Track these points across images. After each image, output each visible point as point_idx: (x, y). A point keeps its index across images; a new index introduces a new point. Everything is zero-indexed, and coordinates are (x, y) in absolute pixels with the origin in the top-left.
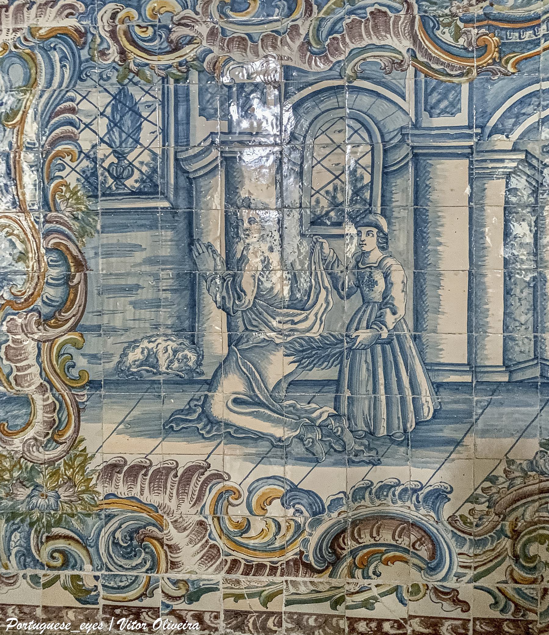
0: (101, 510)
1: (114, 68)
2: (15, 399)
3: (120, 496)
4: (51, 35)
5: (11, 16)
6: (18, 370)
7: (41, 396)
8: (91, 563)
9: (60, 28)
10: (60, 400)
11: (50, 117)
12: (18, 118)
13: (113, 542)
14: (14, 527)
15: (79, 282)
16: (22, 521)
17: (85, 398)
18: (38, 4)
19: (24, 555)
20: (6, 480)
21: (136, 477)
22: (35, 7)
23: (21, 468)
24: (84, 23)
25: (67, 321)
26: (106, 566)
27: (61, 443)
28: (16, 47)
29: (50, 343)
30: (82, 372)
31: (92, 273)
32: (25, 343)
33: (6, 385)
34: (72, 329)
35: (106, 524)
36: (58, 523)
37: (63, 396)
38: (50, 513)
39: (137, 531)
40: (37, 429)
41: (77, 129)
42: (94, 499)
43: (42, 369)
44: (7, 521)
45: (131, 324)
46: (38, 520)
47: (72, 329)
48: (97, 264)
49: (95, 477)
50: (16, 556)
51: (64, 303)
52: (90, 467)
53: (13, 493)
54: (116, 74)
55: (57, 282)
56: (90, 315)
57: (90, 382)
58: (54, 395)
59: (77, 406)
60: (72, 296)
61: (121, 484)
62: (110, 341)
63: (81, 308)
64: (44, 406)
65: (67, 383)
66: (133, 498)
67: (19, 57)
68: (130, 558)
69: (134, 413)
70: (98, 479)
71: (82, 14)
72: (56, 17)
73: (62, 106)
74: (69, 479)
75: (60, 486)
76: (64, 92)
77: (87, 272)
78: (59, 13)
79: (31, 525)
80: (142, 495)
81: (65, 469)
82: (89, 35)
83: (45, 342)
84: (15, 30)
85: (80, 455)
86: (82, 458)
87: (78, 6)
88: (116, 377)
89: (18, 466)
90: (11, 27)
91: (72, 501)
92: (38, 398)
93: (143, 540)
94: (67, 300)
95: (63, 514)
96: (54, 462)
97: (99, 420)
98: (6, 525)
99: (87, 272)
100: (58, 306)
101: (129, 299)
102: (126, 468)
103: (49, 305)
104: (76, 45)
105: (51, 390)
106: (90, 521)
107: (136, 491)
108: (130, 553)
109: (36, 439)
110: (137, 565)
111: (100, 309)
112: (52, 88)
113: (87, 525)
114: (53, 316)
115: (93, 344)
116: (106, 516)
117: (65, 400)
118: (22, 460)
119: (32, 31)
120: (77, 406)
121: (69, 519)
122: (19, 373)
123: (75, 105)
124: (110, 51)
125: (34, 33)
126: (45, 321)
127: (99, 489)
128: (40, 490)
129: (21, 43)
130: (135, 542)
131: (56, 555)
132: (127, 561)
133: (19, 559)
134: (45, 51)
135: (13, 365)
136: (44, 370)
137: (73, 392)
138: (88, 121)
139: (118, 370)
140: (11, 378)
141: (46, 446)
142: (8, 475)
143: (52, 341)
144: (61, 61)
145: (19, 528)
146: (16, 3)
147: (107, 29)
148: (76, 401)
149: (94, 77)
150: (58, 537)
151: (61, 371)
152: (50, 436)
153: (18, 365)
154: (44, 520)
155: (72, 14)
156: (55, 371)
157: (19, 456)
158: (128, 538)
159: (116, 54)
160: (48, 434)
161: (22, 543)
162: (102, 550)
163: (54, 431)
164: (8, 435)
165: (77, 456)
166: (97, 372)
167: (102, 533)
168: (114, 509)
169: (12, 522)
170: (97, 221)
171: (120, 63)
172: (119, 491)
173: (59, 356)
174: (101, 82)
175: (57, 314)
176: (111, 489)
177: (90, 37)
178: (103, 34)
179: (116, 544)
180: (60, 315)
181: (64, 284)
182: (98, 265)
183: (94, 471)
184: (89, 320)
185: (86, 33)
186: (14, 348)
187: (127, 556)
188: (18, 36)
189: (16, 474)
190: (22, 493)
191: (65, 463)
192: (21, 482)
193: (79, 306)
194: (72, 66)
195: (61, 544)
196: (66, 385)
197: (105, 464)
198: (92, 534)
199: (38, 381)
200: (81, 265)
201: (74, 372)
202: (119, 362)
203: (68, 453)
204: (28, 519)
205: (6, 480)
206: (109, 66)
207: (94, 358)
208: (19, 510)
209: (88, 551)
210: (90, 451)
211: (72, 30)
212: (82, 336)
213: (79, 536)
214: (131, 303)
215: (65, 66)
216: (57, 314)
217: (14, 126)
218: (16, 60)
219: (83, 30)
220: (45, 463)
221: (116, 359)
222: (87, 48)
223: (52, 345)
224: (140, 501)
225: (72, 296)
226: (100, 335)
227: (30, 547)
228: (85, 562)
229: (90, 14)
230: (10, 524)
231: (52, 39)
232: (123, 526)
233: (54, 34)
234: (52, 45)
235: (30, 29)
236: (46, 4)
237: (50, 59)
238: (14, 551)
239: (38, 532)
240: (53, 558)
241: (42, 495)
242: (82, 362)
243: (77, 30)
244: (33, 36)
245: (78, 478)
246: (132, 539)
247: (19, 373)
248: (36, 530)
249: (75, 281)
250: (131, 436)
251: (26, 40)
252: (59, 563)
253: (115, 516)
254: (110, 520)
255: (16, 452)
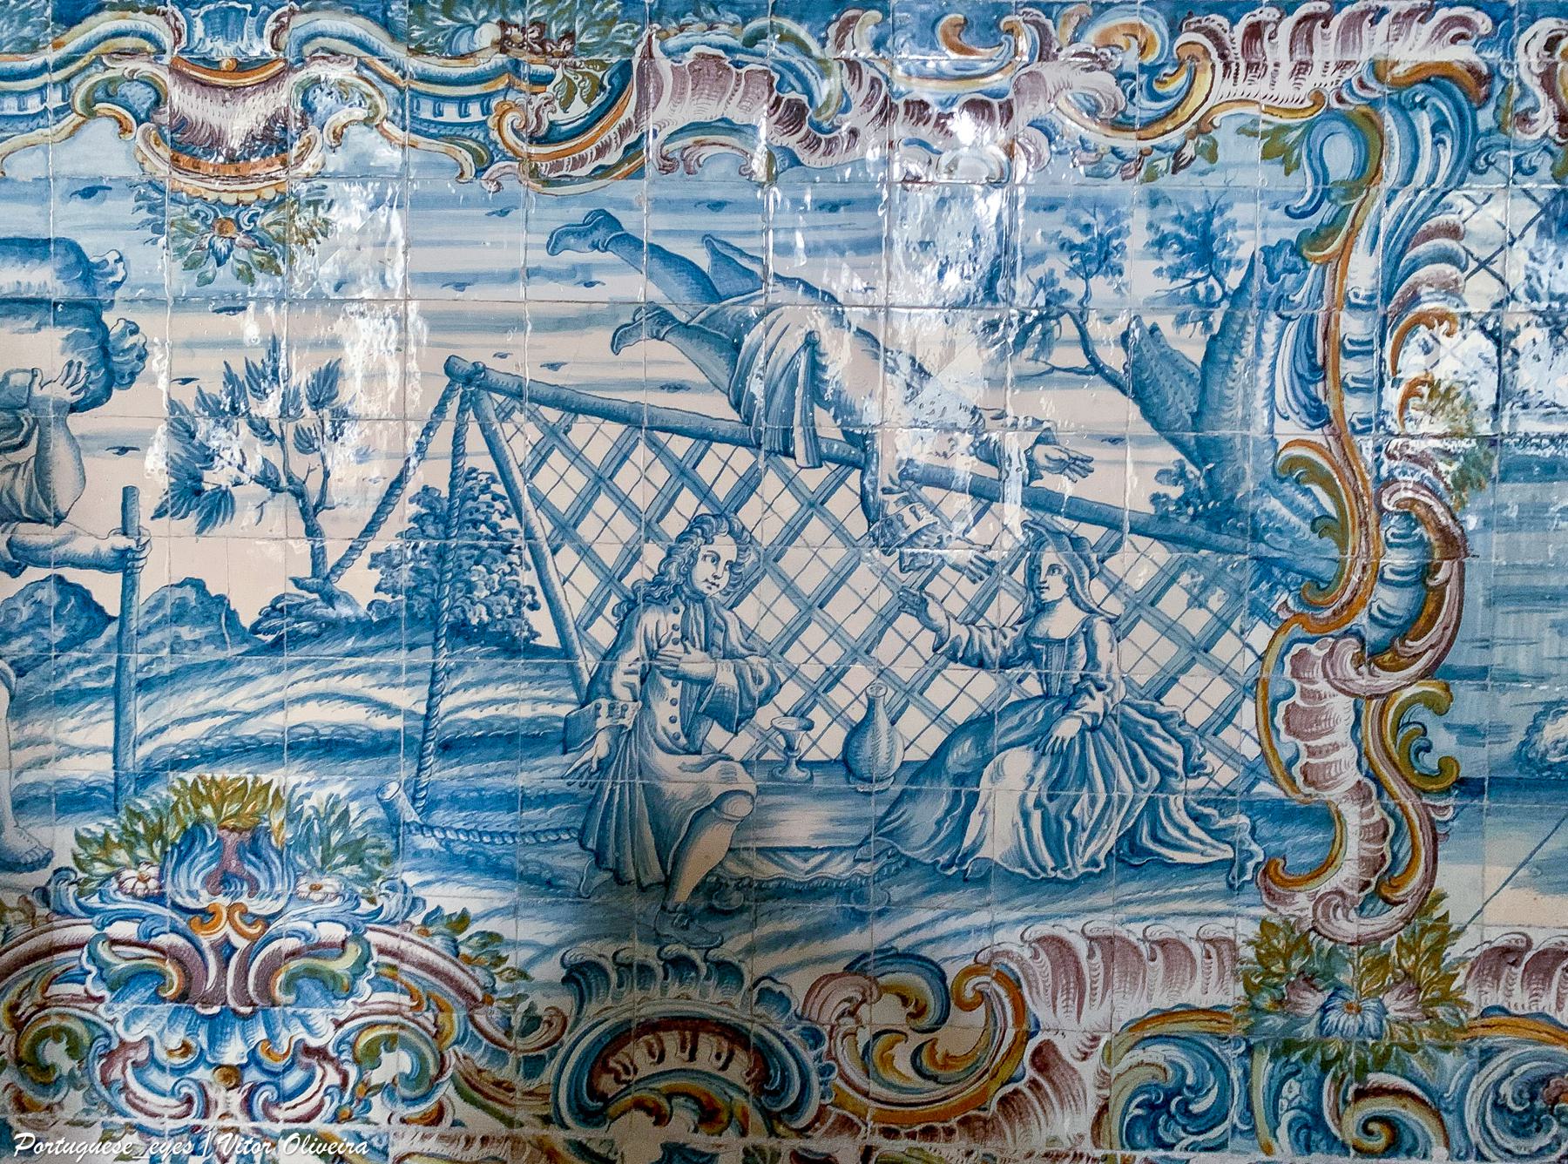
0: (1473, 1039)
1: (1546, 148)
2: (1301, 812)
3: (1513, 1010)
4: (1418, 76)
5: (1334, 36)
6: (1312, 754)
7: (1358, 808)
8: (1447, 1145)
9: (1438, 65)
10: (1398, 816)
11: (1406, 244)
12: (1337, 244)
13: (1495, 1104)
14: (1289, 1069)
15: (1447, 581)
16: (1306, 1058)
17: (1450, 814)
18: (1392, 14)
19: (1306, 1126)
20: (1275, 975)
21: (1549, 975)
22: (1386, 19)
23: (1308, 951)
24: (1489, 55)
25: (1420, 655)
26: (1479, 1151)
27: (1396, 904)
28: (1340, 100)
29: (1380, 701)
30: (1446, 763)
31: (1475, 561)
32: (1329, 700)
33: (1283, 783)
34: (1427, 674)
35: (1482, 1065)
36: (1381, 1064)
37: (1403, 808)
38: (1365, 1043)
39: (1545, 1081)
40: (1346, 874)
41: (1463, 270)
42: (1457, 1016)
43: (1362, 753)
44: (1274, 1057)
45: (1552, 667)
46: (1339, 1056)
47: (1427, 674)
48: (1487, 546)
49: (1463, 972)
50: (1290, 1127)
51: (1413, 619)
52: (1454, 951)
53: (1289, 1001)
54: (1549, 161)
55: (1398, 578)
56: (1467, 647)
57: (1461, 782)
58: (1385, 807)
59: (1433, 829)
60: (1431, 607)
61: (1517, 987)
62: (1506, 700)
63: (1449, 632)
64: (1363, 827)
65: (1414, 781)
66: (1541, 1015)
67: (1346, 119)
68: (1527, 1135)
69: (1548, 847)
70: (1468, 976)
71: (1487, 36)
72: (1430, 41)
73: (1432, 223)
74: (1407, 975)
75: (1388, 989)
76: (1438, 195)
77: (1466, 560)
78: (1438, 34)
79: (1325, 1066)
80: (1559, 1009)
81: (1400, 956)
82: (1497, 79)
83: (1370, 698)
84: (1342, 66)
85: (1433, 928)
86: (1435, 935)
87: (1479, 21)
88: (1515, 773)
89: (1303, 947)
90: (1333, 58)
91: (1411, 1020)
92: (1352, 815)
93: (1556, 1100)
94: (1420, 613)
95: (1391, 1045)
96: (1379, 940)
97: (1477, 857)
98: (1271, 1066)
99: (1466, 560)
100: (1400, 627)
101: (1552, 616)
102: (1528, 957)
103: (1384, 625)
104: (1469, 102)
105: (1380, 795)
106: (1448, 1060)
107: (1547, 1003)
108: (1529, 1123)
109: (1341, 893)
110: (1541, 1149)
111: (1487, 634)
112: (1412, 186)
113: (1443, 1071)
114: (1389, 647)
115: (1470, 703)
116: (1482, 1051)
117: (1408, 818)
118: (1313, 934)
119: (1378, 69)
120: (1433, 829)
121: (1404, 1054)
122: (1312, 761)
123: (1459, 223)
124: (1540, 115)
125: (1382, 73)
126: (1373, 656)
127: (1469, 996)
128: (1347, 995)
129: (1353, 93)
130: (1539, 1104)
131: (1373, 1126)
132: (1521, 1142)
133: (1297, 1135)
134: (1403, 109)
135: (1301, 744)
136: (1367, 754)
137: (1425, 800)
138: (1484, 254)
139: (1522, 756)
140: (1296, 770)
141: (1362, 908)
142: (1281, 965)
143: (1386, 697)
144: (1434, 131)
145: (1298, 1071)
146: (1347, 10)
147: (1538, 71)
148: (1431, 819)
149: (1502, 165)
150: (1380, 1091)
151: (1398, 756)
152: (1372, 888)
153: (1311, 743)
154: (1352, 1056)
155: (1462, 36)
156: (1390, 758)
157: (1306, 926)
158: (1526, 1095)
159: (1551, 120)
160: (1368, 884)
161: (1305, 1103)
162: (1470, 1118)
163: (1380, 885)
164: (1285, 883)
165: (1429, 928)
166: (1475, 761)
167: (1473, 1086)
168: (1497, 1038)
169: (1284, 1059)
170: (1492, 457)
171: (1559, 140)
172: (1513, 1001)
173: (1397, 727)
174: (1518, 176)
175: (1397, 643)
176: (1495, 997)
177: (1499, 86)
178: (1526, 78)
179: (1499, 1107)
180: (1403, 644)
181: (1415, 583)
182: (1491, 551)
183: (1462, 961)
184: (1463, 656)
185: (1491, 76)
186: (1304, 710)
187: (1520, 1131)
188: (1346, 77)
189: (1296, 964)
190: (1312, 1001)
191: (1401, 943)
192: (1305, 980)
193: (1446, 628)
194: (1457, 144)
195: (1384, 1106)
196: (1410, 785)
197: (1486, 946)
198: (1452, 1088)
199: (1352, 776)
200: (1454, 544)
201: (1430, 761)
202: (1523, 744)
203: (1408, 923)
204: (1318, 1055)
205: (1275, 975)
206: (1537, 143)
207: (1470, 733)
208: (1300, 1034)
209: (1441, 1121)
210: (1455, 921)
211: (1463, 69)
212: (1447, 689)
213: (1424, 1089)
214: (1553, 625)
215: (1442, 141)
216: (1397, 643)
217: (1327, 261)
218: (1341, 126)
219: (1485, 70)
220: (1359, 943)
221: (1518, 737)
222: (1491, 106)
223: (1384, 704)
224: (1555, 1022)
225: (1431, 607)
226: (1484, 688)
227: (1321, 1109)
228: (1433, 1140)
229: (1503, 37)
230: (1279, 1064)
231: (1419, 87)
232: (1517, 1072)
233: (1424, 75)
234: (1418, 99)
235: (1373, 65)
236: (1411, 14)
237: (1412, 126)
238: (1285, 1119)
239: (1339, 1081)
240: (1369, 1133)
241: (1350, 1007)
242: (1444, 742)
243: (1472, 70)
244: (1379, 79)
245: (1426, 973)
246: (1533, 1098)
247: (1312, 761)
248: (1335, 1077)
249: (1441, 576)
250: (1544, 893)
251: (1363, 86)
252: (1380, 1143)
253: (1501, 1050)
254: (1489, 1059)
255: (1300, 919)
